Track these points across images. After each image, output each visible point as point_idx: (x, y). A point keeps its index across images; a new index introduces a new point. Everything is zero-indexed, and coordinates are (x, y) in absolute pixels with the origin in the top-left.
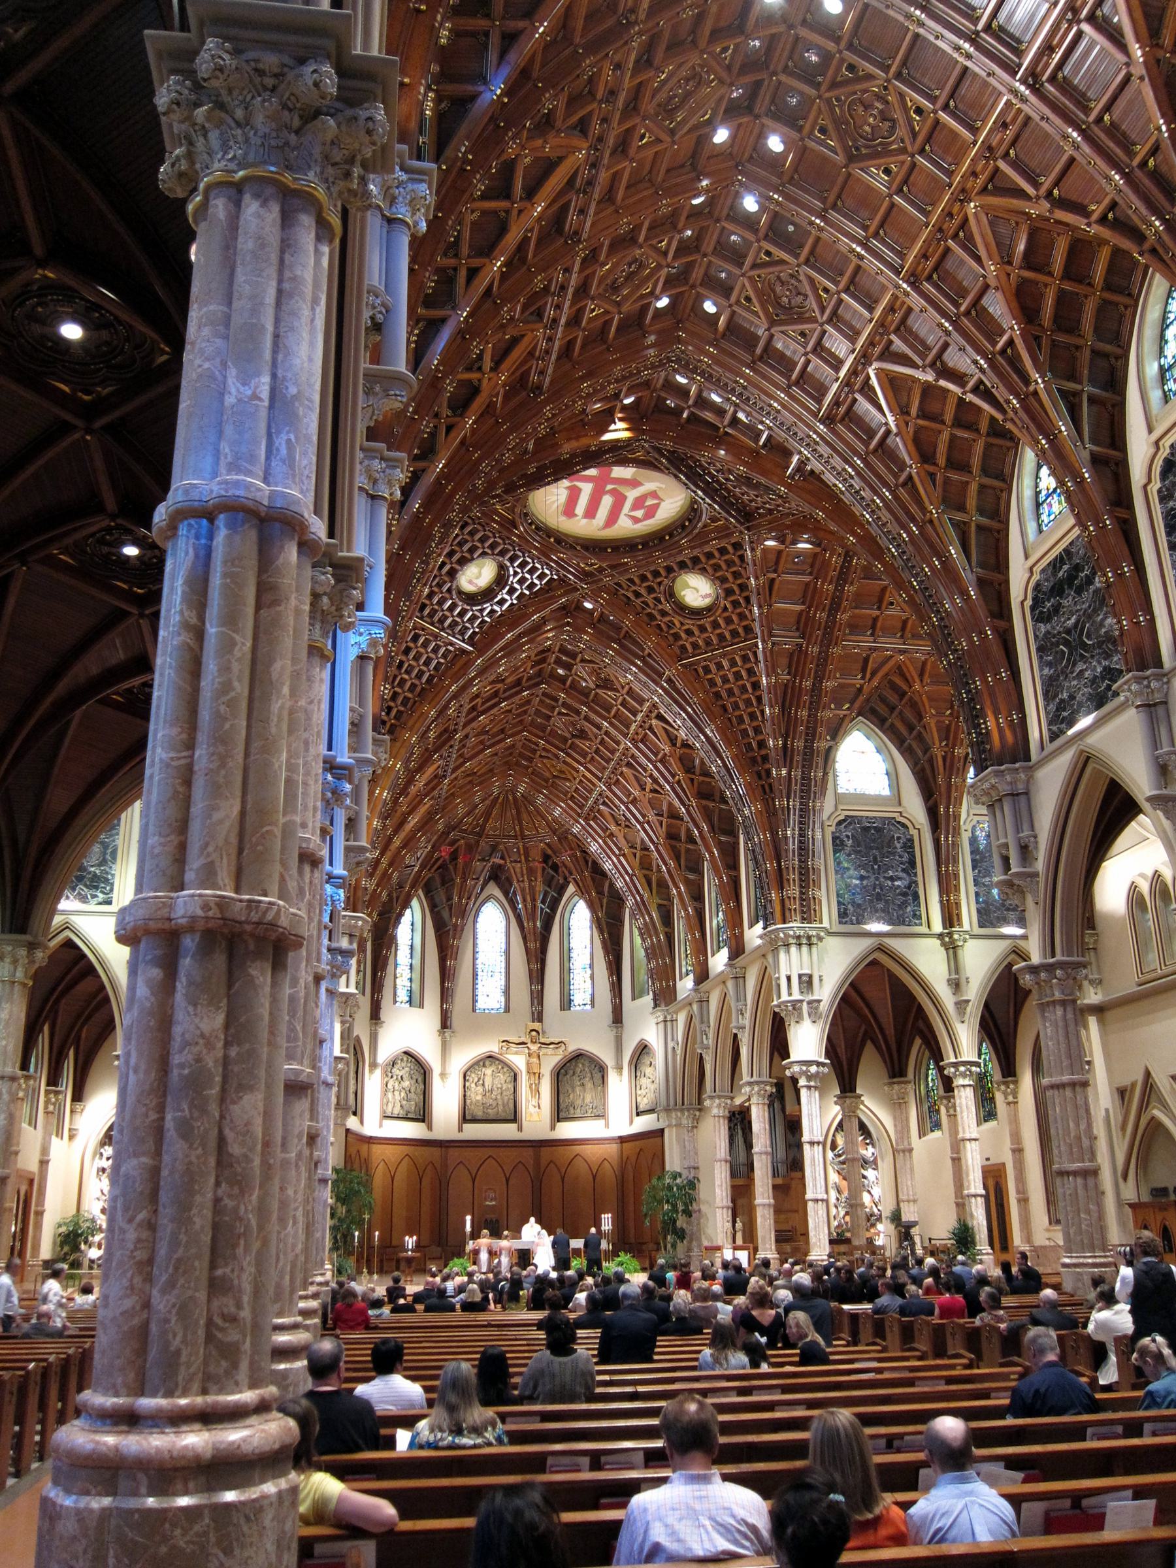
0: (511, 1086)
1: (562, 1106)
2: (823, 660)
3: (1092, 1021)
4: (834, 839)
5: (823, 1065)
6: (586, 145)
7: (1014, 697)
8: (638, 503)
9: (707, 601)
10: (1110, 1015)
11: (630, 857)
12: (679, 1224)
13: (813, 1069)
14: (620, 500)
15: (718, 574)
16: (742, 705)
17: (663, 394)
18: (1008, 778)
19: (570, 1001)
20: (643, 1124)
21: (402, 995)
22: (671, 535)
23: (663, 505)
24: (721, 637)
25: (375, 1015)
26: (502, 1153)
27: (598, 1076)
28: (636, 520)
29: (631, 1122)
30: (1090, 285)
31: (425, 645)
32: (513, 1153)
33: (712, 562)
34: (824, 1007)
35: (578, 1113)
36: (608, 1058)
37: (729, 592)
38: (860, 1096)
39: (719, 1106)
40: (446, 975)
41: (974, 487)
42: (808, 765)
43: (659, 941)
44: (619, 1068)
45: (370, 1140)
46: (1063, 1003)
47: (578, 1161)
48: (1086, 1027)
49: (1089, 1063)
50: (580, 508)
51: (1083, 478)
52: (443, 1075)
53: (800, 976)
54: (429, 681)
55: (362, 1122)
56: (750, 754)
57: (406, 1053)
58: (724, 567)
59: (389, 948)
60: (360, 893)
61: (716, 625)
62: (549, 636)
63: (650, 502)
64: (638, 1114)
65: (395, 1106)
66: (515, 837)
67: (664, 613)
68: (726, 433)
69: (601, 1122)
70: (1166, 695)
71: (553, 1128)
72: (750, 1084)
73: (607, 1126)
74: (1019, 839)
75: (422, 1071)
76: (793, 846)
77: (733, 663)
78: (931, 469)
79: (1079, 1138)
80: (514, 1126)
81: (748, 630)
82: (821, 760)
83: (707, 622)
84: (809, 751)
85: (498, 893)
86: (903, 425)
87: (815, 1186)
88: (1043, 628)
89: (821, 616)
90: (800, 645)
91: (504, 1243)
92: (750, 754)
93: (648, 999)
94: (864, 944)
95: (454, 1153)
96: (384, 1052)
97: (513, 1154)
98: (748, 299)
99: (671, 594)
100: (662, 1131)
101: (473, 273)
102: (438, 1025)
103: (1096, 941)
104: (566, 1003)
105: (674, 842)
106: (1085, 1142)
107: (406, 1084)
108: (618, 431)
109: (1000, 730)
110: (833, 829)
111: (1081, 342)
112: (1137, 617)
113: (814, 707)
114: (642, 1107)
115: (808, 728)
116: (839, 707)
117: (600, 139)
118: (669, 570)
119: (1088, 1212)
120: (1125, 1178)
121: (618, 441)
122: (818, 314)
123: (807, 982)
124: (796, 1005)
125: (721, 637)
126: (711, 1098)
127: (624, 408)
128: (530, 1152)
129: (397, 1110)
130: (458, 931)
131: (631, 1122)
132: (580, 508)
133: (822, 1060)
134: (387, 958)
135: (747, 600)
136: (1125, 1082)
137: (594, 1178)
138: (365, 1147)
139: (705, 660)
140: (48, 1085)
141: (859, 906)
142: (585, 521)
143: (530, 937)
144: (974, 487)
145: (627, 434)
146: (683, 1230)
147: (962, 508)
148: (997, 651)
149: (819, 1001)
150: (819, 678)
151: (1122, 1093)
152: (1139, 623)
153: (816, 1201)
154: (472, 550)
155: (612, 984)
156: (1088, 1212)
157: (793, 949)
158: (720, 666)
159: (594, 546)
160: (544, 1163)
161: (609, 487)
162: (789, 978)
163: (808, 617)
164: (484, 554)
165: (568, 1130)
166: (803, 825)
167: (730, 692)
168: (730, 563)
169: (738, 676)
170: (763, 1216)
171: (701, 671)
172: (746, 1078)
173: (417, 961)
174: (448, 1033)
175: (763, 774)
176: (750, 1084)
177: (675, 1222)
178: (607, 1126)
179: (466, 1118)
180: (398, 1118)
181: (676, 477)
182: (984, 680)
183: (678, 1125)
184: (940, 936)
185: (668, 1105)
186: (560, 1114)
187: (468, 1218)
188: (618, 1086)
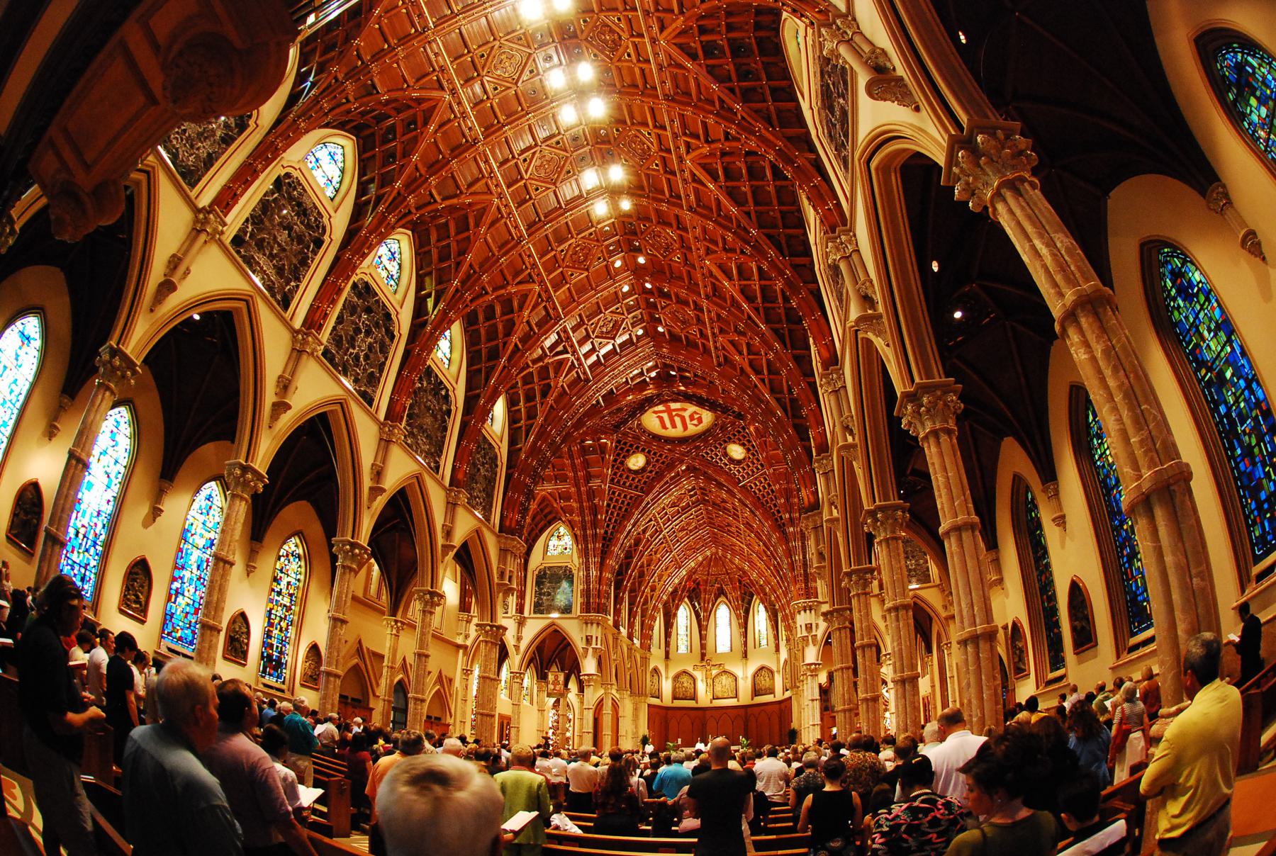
8: (692, 418)
14: (683, 419)
28: (696, 425)
31: (619, 495)
34: (819, 637)
36: (775, 669)
37: (748, 450)
50: (668, 424)
54: (626, 510)
61: (749, 466)
63: (696, 416)
67: (726, 465)
78: (761, 377)
95: (749, 710)
101: (505, 344)
128: (777, 706)
132: (668, 424)
157: (595, 625)
158: (756, 485)
159: (682, 441)
164: (634, 453)
166: (588, 576)
167: (763, 496)
169: (764, 487)
179: (675, 698)
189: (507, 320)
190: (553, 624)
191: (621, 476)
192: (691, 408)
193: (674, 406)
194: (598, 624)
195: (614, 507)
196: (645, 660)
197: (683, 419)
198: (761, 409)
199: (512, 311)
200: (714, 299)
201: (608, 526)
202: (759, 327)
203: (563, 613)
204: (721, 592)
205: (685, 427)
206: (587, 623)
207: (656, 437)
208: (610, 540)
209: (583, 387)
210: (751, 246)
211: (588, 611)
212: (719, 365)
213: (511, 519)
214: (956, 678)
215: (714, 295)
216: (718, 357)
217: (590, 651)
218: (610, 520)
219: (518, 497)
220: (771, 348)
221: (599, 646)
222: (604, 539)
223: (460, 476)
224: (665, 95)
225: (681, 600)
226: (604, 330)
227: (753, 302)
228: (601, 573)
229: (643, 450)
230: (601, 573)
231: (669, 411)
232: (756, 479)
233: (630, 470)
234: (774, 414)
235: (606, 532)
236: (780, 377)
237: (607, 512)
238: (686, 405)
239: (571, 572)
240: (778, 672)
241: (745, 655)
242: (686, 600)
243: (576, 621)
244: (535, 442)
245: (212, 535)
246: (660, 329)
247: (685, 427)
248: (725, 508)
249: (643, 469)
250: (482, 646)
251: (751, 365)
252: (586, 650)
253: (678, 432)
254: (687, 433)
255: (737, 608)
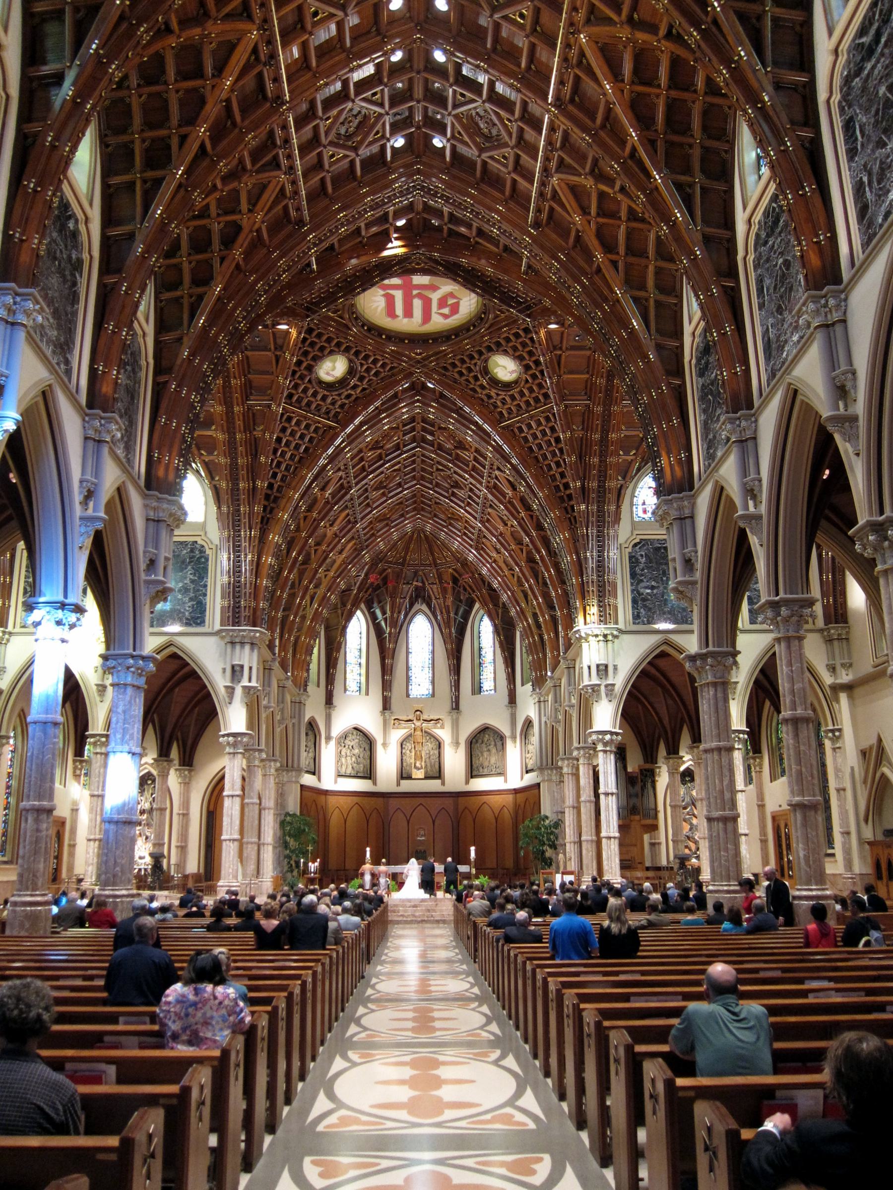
0: (436, 752)
1: (475, 766)
2: (607, 417)
3: (843, 697)
4: (631, 558)
5: (617, 734)
6: (255, 27)
7: (683, 441)
8: (442, 303)
9: (514, 376)
10: (858, 691)
11: (511, 577)
12: (548, 854)
13: (608, 737)
14: (427, 303)
15: (517, 354)
16: (549, 456)
17: (425, 216)
18: (675, 505)
19: (481, 687)
20: (530, 779)
21: (352, 685)
22: (474, 326)
23: (462, 303)
24: (527, 403)
25: (329, 700)
26: (429, 801)
27: (499, 744)
28: (446, 317)
29: (522, 778)
30: (695, 91)
31: (298, 423)
32: (438, 801)
33: (511, 344)
34: (618, 688)
35: (486, 771)
36: (506, 730)
37: (527, 368)
38: (682, 757)
39: (568, 765)
40: (386, 671)
41: (651, 269)
42: (601, 500)
43: (534, 641)
44: (514, 737)
45: (326, 793)
46: (715, 684)
47: (485, 806)
48: (838, 701)
49: (840, 730)
50: (399, 309)
51: (696, 256)
52: (385, 745)
53: (598, 666)
54: (306, 449)
55: (319, 779)
56: (559, 494)
57: (355, 729)
58: (520, 348)
59: (338, 650)
60: (259, 613)
61: (522, 394)
62: (405, 412)
63: (451, 301)
64: (527, 772)
65: (348, 765)
66: (430, 565)
67: (482, 387)
68: (477, 243)
69: (502, 778)
70: (756, 430)
71: (467, 782)
72: (578, 749)
73: (506, 781)
74: (684, 555)
75: (368, 742)
76: (591, 564)
77: (539, 424)
78: (613, 257)
79: (722, 792)
80: (438, 782)
81: (546, 396)
82: (615, 497)
83: (515, 392)
84: (602, 491)
85: (424, 607)
86: (586, 223)
87: (608, 826)
88: (701, 381)
89: (601, 382)
90: (588, 406)
91: (382, 868)
92: (559, 494)
93: (529, 686)
94: (653, 640)
95: (394, 803)
96: (337, 730)
97: (438, 802)
98: (459, 133)
99: (486, 371)
100: (538, 785)
101: (183, 138)
102: (381, 708)
103: (848, 633)
104: (477, 689)
105: (532, 565)
106: (727, 795)
107: (356, 751)
108: (395, 248)
109: (671, 466)
110: (630, 550)
111: (691, 141)
112: (735, 368)
113: (603, 455)
114: (529, 767)
115: (600, 471)
116: (627, 453)
117: (265, 21)
118: (480, 353)
119: (726, 850)
120: (866, 821)
121: (395, 256)
122: (507, 138)
123: (602, 670)
124: (595, 688)
125: (527, 403)
126: (563, 759)
127: (398, 230)
129: (349, 771)
130: (396, 638)
131: (522, 778)
132: (399, 309)
133: (745, 728)
134: (336, 659)
135: (542, 372)
136: (865, 745)
137: (496, 819)
138: (323, 797)
139: (518, 422)
140: (76, 755)
141: (650, 609)
142: (406, 320)
143: (448, 640)
144: (651, 269)
145: (402, 250)
146: (551, 859)
147: (643, 287)
148: (671, 404)
149: (613, 685)
150: (605, 432)
151: (864, 753)
152: (736, 373)
153: (609, 838)
154: (322, 349)
155: (508, 674)
156: (726, 850)
158: (529, 427)
160: (461, 808)
161: (415, 292)
162: (589, 667)
163: (592, 384)
164: (331, 353)
165: (481, 784)
166: (601, 549)
168: (524, 345)
170: (587, 849)
171: (516, 430)
172: (575, 744)
173: (363, 661)
174: (387, 713)
175: (569, 509)
176: (578, 749)
177: (543, 852)
178: (506, 781)
180: (350, 776)
181: (455, 280)
182: (660, 427)
183: (550, 780)
184: (821, 631)
185: (543, 766)
186: (473, 771)
187: (473, 849)
188: (513, 753)
189: (188, 91)
190: (170, 644)
191: (305, 391)
192: (447, 287)
193: (419, 280)
194: (252, 644)
195: (287, 444)
196: (299, 705)
197: (427, 303)
198: (603, 311)
199: (199, 73)
200: (570, 108)
201: (275, 475)
202: (649, 176)
203: (188, 624)
204: (420, 596)
205: (427, 316)
206: (233, 643)
207: (374, 330)
208: (276, 499)
209: (290, 236)
210: (700, 31)
211: (236, 623)
212: (537, 224)
213: (167, 467)
214: (849, 793)
215: (572, 100)
216: (539, 210)
217: (239, 691)
218: (279, 464)
219: (178, 427)
220: (666, 216)
221: (254, 684)
222: (267, 497)
223: (106, 388)
224: (558, 98)
225: (355, 606)
226: (343, 131)
227: (648, 128)
228: (259, 558)
229: (347, 350)
230: (259, 558)
231: (407, 289)
232: (532, 417)
233: (320, 382)
234: (625, 323)
235: (271, 486)
236: (643, 261)
237: (275, 451)
238: (437, 280)
239: (202, 550)
240: (514, 737)
241: (456, 706)
242: (363, 606)
243: (213, 640)
244: (205, 329)
245: (356, 751)
246: (437, 142)
247: (427, 316)
248: (458, 457)
249: (342, 383)
250: (110, 689)
251: (599, 235)
252: (231, 691)
253: (412, 324)
254: (429, 328)
255: (448, 625)
